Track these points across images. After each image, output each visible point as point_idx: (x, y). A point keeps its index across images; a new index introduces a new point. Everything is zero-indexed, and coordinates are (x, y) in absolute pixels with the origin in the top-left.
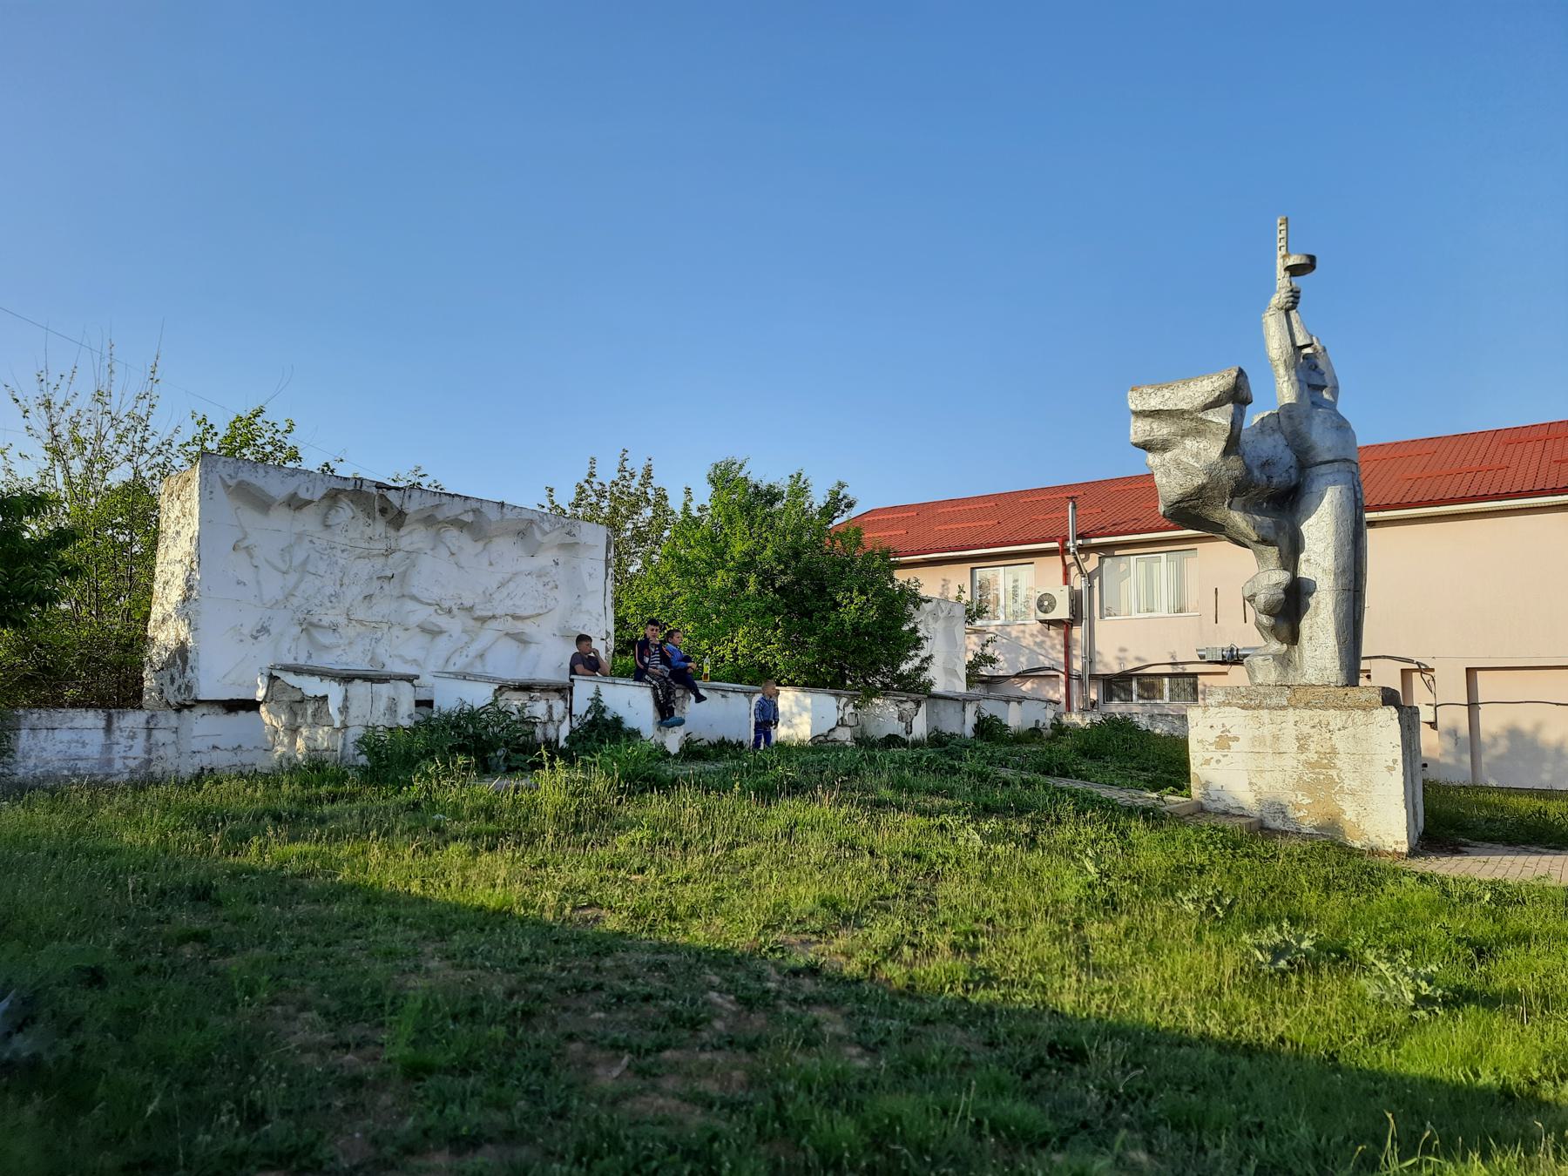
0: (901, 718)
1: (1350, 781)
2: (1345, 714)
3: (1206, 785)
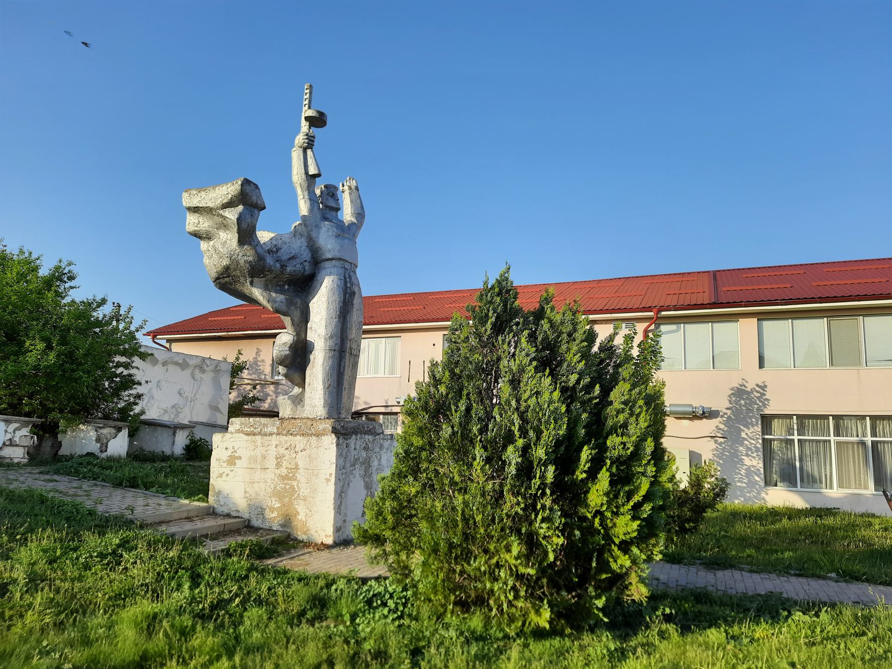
0: (98, 440)
1: (304, 491)
2: (305, 439)
3: (219, 493)
